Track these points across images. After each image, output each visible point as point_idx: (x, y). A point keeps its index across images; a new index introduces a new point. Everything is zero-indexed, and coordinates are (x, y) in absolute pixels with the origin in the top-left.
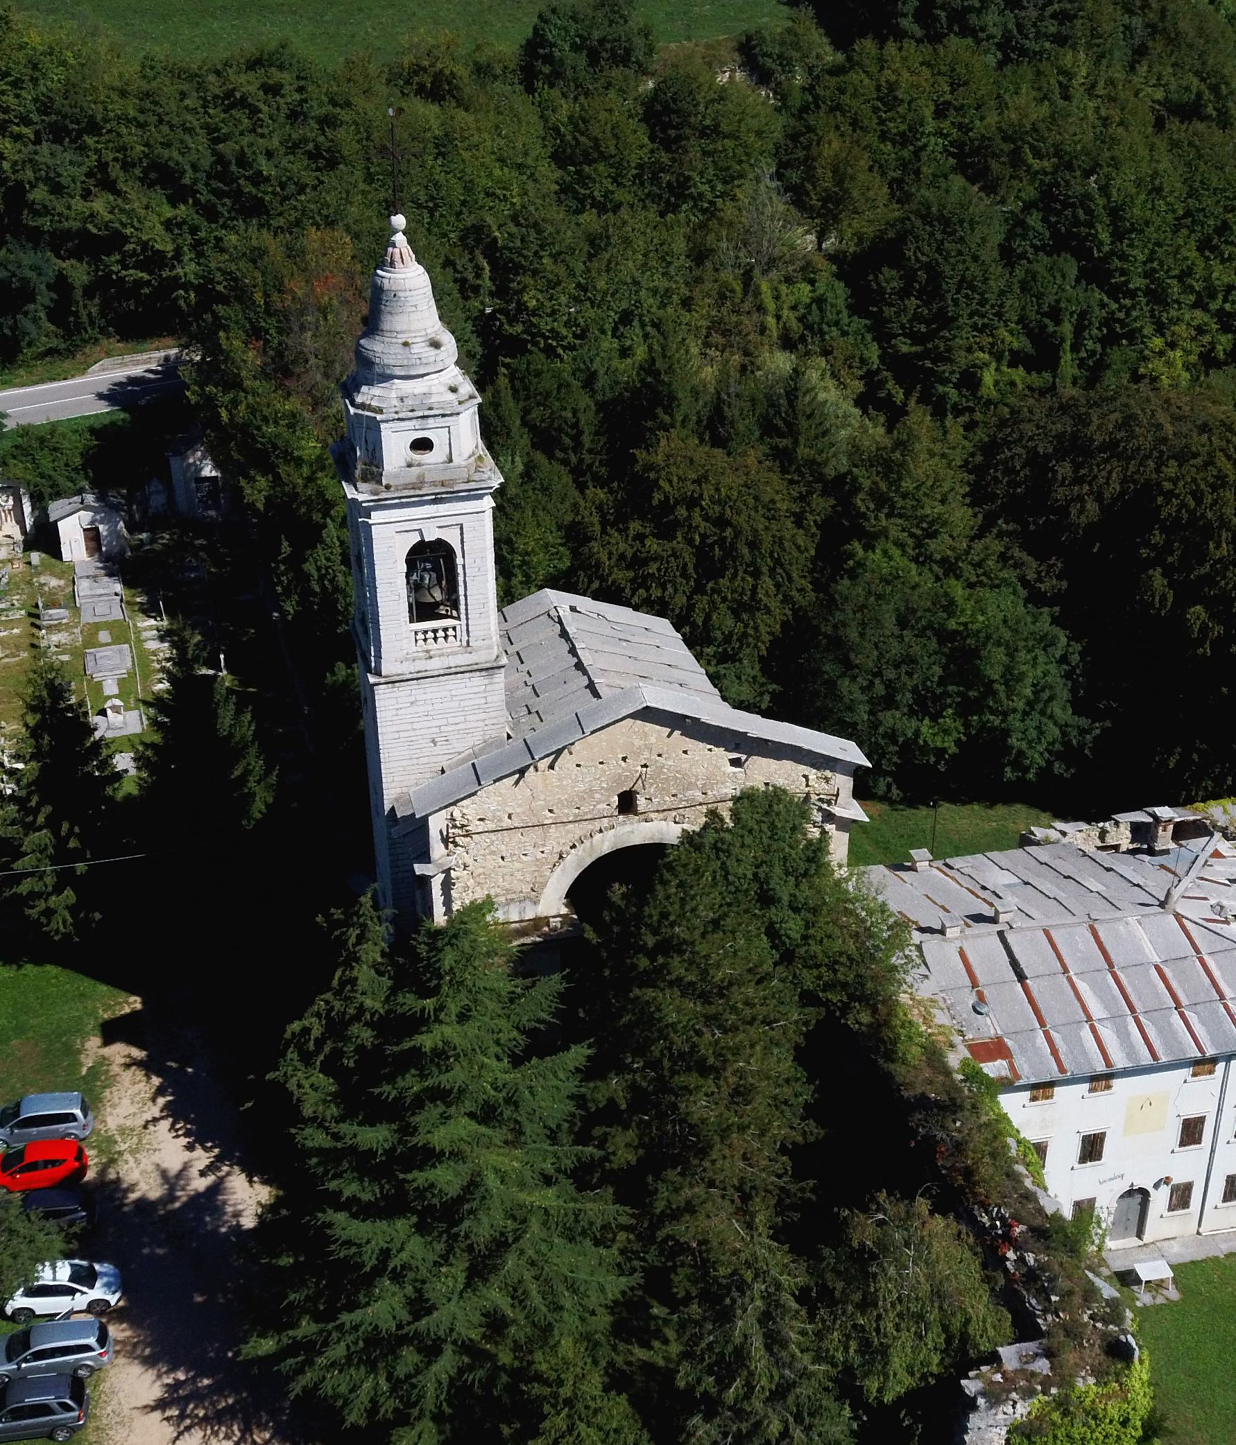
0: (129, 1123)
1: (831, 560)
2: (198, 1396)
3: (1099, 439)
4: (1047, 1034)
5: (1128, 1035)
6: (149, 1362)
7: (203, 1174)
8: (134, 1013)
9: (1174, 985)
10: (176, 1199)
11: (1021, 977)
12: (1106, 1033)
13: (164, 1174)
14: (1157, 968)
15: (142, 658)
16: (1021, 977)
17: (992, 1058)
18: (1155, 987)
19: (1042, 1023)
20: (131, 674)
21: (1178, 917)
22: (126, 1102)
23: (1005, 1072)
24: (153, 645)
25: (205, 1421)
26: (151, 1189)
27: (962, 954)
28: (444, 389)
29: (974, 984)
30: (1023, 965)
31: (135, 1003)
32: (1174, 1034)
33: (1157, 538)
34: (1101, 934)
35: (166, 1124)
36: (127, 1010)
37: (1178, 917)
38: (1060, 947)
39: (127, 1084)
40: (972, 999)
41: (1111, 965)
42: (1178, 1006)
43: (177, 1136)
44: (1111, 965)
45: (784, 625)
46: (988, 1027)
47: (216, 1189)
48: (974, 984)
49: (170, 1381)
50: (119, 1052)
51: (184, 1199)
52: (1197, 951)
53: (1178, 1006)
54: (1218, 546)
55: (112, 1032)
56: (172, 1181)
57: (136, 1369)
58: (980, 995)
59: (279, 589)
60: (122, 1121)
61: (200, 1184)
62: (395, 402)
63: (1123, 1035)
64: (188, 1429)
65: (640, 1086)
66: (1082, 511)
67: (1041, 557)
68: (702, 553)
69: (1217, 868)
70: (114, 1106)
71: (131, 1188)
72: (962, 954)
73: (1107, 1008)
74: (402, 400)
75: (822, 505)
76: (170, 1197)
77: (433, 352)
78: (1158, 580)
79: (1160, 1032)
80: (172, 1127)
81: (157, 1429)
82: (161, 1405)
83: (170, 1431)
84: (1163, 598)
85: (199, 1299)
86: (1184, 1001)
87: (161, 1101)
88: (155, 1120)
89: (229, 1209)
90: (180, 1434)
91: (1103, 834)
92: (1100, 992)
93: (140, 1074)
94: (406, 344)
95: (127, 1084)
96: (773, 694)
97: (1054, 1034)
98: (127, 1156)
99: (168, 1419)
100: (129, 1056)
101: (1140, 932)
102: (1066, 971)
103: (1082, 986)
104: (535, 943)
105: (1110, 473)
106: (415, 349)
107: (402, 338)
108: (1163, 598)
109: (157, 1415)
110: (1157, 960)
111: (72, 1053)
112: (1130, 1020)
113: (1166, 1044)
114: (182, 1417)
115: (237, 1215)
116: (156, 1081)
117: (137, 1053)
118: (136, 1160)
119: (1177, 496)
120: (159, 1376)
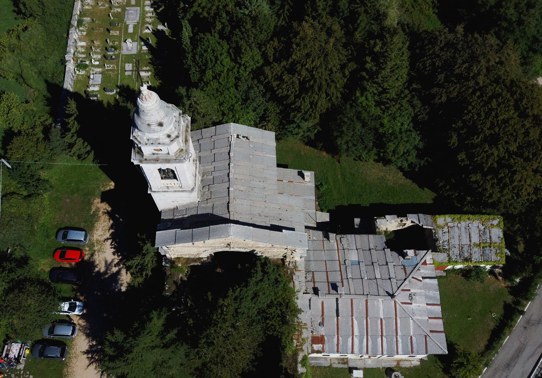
0: (99, 238)
1: (354, 84)
2: (97, 352)
3: (457, 71)
4: (338, 337)
5: (362, 342)
6: (88, 335)
7: (115, 266)
8: (110, 190)
9: (384, 327)
10: (107, 273)
11: (338, 315)
12: (356, 341)
13: (106, 261)
14: (381, 319)
15: (143, 14)
16: (338, 315)
17: (318, 343)
18: (377, 326)
19: (338, 334)
20: (138, 23)
21: (395, 302)
22: (100, 229)
23: (320, 349)
24: (148, 9)
25: (97, 361)
26: (101, 267)
27: (323, 303)
28: (165, 137)
29: (323, 315)
30: (340, 312)
31: (112, 185)
32: (377, 345)
33: (460, 124)
34: (369, 304)
35: (110, 241)
36: (108, 189)
37: (395, 302)
38: (354, 306)
39: (102, 221)
40: (320, 320)
41: (367, 316)
42: (382, 336)
43: (111, 248)
44: (367, 316)
45: (327, 109)
46: (322, 331)
47: (118, 273)
48: (323, 315)
49: (91, 344)
50: (105, 207)
51: (109, 274)
52: (396, 316)
53: (382, 336)
54: (477, 138)
55: (105, 197)
56: (108, 266)
57: (84, 337)
58: (323, 319)
59: (180, 17)
60: (98, 237)
61: (115, 269)
62: (146, 141)
63: (361, 342)
64: (92, 362)
65: (293, 124)
66: (440, 99)
67: (424, 104)
68: (302, 83)
69: (422, 271)
70: (97, 230)
71: (96, 266)
72: (323, 303)
73: (360, 332)
74: (148, 140)
75: (353, 66)
76: (105, 273)
77: (159, 128)
78: (454, 139)
79: (373, 343)
80: (111, 244)
81: (83, 360)
82: (87, 352)
83: (87, 362)
84: (453, 144)
85: (105, 315)
86: (384, 334)
87: (111, 231)
88: (108, 239)
89: (120, 282)
90: (90, 364)
91: (401, 221)
92: (360, 324)
93: (107, 217)
94: (149, 125)
95: (102, 221)
96: (318, 131)
97: (340, 338)
98: (96, 253)
99: (88, 358)
100: (106, 209)
101: (381, 306)
102: (352, 316)
103: (355, 322)
104: (198, 265)
105: (456, 88)
106: (152, 127)
107: (147, 123)
108: (453, 144)
109: (85, 356)
110: (382, 317)
111: (90, 204)
112: (365, 337)
113: (372, 348)
114: (92, 358)
115: (121, 285)
116: (111, 222)
117: (110, 209)
118: (99, 255)
119: (472, 113)
120: (89, 342)
